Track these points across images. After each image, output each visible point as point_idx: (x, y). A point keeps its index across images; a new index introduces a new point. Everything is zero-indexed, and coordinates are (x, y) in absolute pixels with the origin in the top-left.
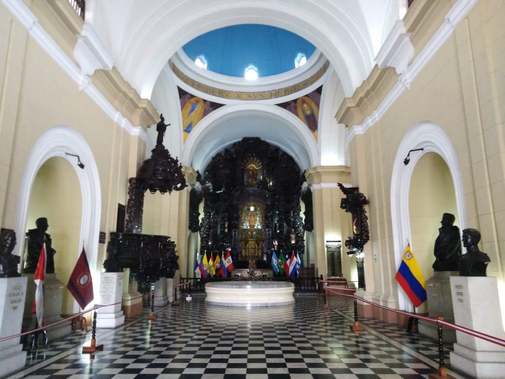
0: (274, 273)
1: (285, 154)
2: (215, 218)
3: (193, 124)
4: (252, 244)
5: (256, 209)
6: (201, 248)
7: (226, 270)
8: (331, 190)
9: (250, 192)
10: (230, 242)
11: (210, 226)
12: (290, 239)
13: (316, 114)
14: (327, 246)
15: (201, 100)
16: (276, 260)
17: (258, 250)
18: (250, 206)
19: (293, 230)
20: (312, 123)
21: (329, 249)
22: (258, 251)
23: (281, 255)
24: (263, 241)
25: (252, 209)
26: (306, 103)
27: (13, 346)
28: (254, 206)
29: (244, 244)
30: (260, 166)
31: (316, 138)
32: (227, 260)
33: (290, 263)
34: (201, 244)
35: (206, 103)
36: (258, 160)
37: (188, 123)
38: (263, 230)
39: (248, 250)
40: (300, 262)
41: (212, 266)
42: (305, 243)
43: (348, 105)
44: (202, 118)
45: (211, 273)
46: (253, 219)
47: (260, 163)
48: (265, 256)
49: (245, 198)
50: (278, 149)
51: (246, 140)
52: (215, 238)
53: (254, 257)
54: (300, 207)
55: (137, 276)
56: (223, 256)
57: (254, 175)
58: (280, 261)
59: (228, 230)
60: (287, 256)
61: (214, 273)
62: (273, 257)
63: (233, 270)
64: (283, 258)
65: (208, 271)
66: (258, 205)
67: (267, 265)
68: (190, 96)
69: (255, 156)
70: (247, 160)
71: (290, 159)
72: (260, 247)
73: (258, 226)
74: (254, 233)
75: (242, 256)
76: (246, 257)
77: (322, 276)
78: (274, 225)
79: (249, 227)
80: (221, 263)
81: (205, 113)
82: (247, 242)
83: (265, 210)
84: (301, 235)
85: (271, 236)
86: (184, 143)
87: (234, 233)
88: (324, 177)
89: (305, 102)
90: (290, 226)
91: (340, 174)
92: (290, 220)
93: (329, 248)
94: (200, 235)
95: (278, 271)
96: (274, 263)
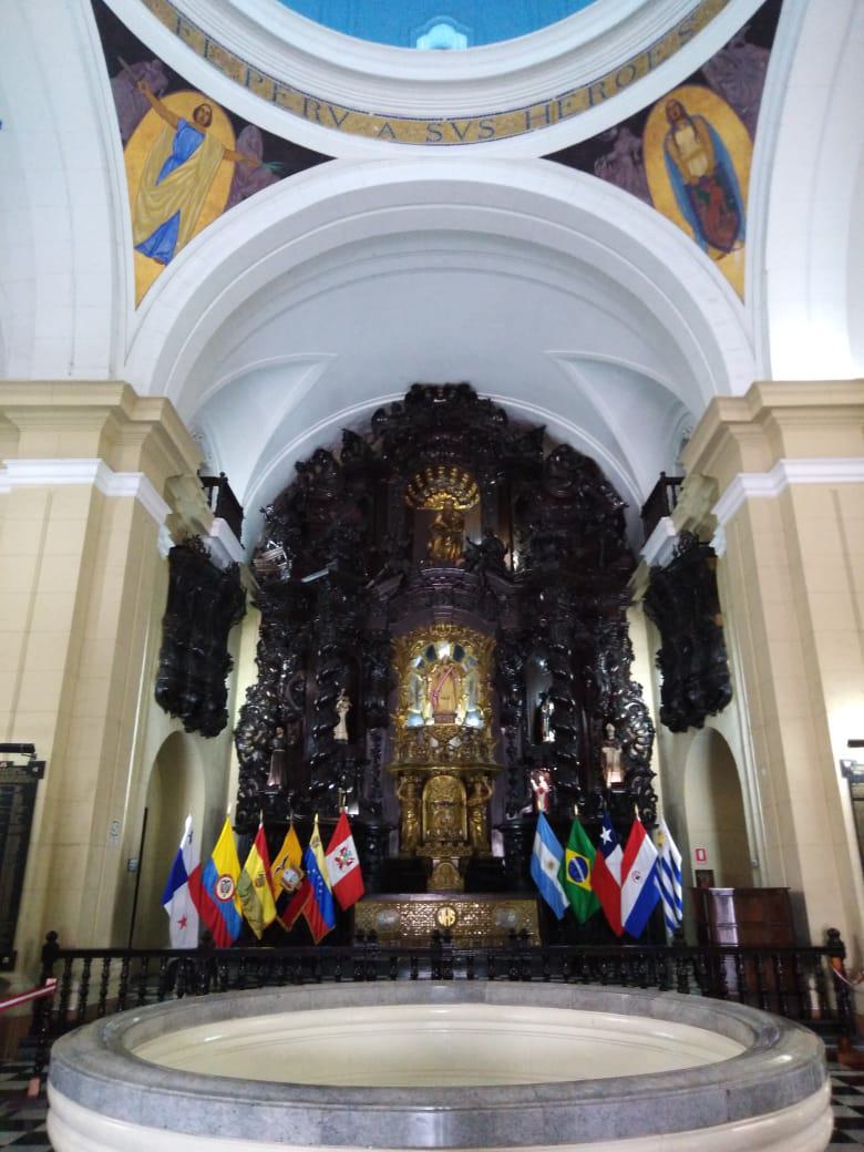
0: (546, 912)
1: (566, 451)
2: (296, 684)
3: (185, 229)
4: (443, 786)
5: (458, 654)
6: (239, 808)
7: (329, 902)
8: (835, 493)
9: (438, 586)
10: (357, 783)
11: (277, 715)
12: (598, 766)
14: (846, 772)
16: (554, 853)
18: (436, 639)
19: (611, 727)
20: (716, 213)
22: (470, 816)
23: (578, 829)
24: (488, 774)
25: (445, 651)
26: (690, 121)
27: (106, 976)
28: (451, 639)
29: (410, 789)
30: (473, 497)
32: (336, 853)
33: (626, 866)
34: (242, 789)
36: (466, 478)
37: (165, 214)
38: (489, 734)
39: (430, 815)
41: (260, 883)
42: (656, 783)
43: (725, 416)
45: (253, 915)
46: (447, 687)
47: (474, 487)
48: (500, 836)
50: (536, 434)
51: (418, 394)
53: (455, 845)
54: (630, 644)
55: (467, 862)
56: (316, 833)
58: (571, 855)
59: (349, 729)
60: (606, 835)
61: (270, 915)
62: (538, 837)
63: (361, 899)
64: (588, 843)
65: (238, 908)
66: (468, 636)
68: (163, 81)
69: (454, 461)
71: (589, 467)
72: (478, 799)
73: (469, 716)
74: (453, 742)
76: (421, 843)
79: (431, 723)
80: (304, 865)
81: (241, 189)
82: (427, 777)
83: (495, 653)
85: (519, 755)
86: (137, 306)
87: (370, 744)
88: (790, 438)
89: (684, 115)
90: (597, 716)
92: (599, 689)
95: (566, 903)
96: (543, 866)
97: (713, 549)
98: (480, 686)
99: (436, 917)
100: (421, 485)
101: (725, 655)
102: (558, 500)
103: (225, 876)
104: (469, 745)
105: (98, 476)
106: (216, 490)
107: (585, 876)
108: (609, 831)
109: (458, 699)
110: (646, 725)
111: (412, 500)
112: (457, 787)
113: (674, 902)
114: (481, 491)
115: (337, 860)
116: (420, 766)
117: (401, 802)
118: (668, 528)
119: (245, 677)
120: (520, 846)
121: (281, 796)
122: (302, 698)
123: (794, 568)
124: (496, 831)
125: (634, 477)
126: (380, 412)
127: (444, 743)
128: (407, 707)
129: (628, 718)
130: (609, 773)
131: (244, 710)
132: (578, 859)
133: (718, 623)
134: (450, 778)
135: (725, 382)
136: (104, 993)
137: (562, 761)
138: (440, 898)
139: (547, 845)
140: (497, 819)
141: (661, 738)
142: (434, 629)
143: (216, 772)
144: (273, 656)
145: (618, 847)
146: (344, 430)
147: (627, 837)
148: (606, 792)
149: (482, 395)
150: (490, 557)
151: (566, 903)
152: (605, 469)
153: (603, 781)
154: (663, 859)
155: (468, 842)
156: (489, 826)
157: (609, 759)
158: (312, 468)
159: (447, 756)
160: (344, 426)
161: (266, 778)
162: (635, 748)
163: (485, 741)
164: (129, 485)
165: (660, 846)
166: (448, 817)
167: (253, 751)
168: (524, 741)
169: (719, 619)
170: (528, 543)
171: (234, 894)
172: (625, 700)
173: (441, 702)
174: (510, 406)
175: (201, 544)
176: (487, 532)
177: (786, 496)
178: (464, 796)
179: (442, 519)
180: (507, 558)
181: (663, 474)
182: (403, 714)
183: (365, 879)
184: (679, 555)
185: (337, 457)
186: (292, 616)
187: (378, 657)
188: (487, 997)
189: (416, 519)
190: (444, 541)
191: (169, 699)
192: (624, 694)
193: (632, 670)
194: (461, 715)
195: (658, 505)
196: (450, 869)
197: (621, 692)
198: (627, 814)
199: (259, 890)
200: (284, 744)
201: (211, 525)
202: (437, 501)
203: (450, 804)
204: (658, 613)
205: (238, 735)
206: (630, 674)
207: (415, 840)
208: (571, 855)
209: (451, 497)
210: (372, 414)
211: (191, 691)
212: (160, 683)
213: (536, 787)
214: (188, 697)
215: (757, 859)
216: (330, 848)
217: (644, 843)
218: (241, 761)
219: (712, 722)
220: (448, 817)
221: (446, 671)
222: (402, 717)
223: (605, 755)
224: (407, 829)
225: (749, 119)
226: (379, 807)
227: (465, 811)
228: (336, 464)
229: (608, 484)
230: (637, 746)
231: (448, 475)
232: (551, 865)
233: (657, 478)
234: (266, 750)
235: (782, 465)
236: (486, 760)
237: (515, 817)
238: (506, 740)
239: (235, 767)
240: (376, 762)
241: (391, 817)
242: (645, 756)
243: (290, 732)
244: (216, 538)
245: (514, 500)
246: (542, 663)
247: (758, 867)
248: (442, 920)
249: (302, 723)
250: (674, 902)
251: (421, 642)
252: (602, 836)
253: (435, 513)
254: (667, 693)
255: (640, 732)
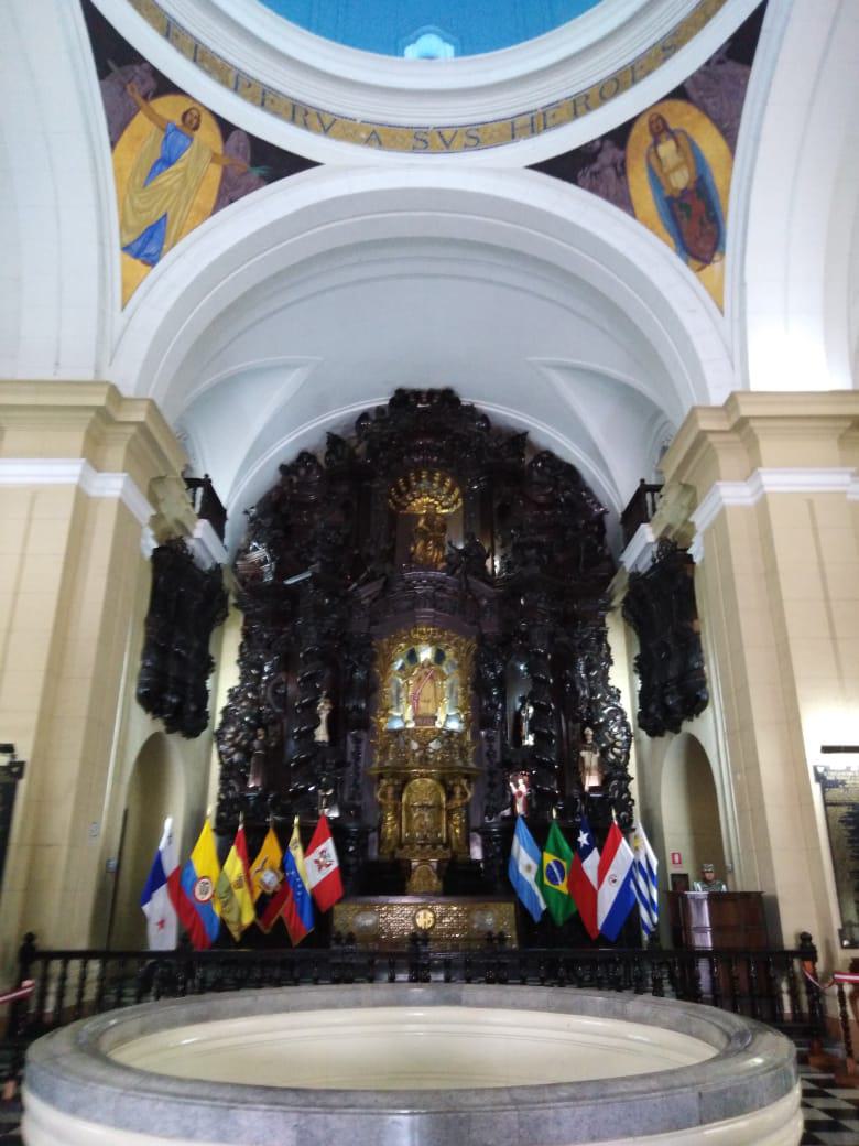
0: (523, 914)
1: (548, 458)
2: (277, 686)
3: (172, 230)
4: (423, 789)
5: (439, 657)
6: (220, 809)
8: (810, 503)
9: (420, 590)
10: (337, 785)
11: (258, 716)
12: (576, 770)
13: (718, 180)
14: (820, 778)
15: (206, 120)
16: (531, 854)
17: (450, 813)
18: (418, 642)
19: (589, 732)
20: (697, 225)
21: (834, 794)
22: (449, 818)
23: (556, 832)
24: (467, 777)
25: (426, 654)
26: (672, 135)
27: (83, 977)
28: (432, 642)
29: (390, 791)
30: (456, 502)
31: (717, 297)
32: (315, 855)
35: (234, 135)
36: (448, 482)
38: (469, 738)
39: (409, 817)
40: (655, 863)
41: (239, 885)
42: (633, 787)
43: (704, 425)
44: (216, 209)
45: (231, 917)
46: (427, 690)
47: (457, 492)
48: (478, 838)
49: (394, 612)
50: (519, 440)
51: (402, 398)
52: (273, 765)
53: (434, 847)
54: (609, 648)
55: (446, 865)
56: (296, 835)
57: (437, 527)
58: (549, 859)
59: (331, 730)
60: (583, 839)
61: (248, 917)
62: (516, 841)
63: (340, 901)
64: (566, 847)
65: (217, 909)
66: (449, 640)
67: (490, 880)
68: (151, 84)
69: (438, 466)
70: (407, 483)
71: (570, 473)
73: (449, 718)
74: (434, 745)
75: (381, 842)
76: (401, 845)
77: (805, 938)
78: (510, 716)
79: (411, 725)
81: (229, 193)
82: (407, 780)
84: (618, 757)
85: (498, 760)
87: (351, 746)
88: (767, 447)
89: (665, 128)
90: (576, 720)
91: (842, 438)
92: (578, 693)
93: (835, 784)
94: (220, 753)
95: (543, 906)
96: (521, 869)
97: (691, 556)
98: (460, 689)
99: (414, 919)
100: (404, 489)
101: (701, 660)
102: (540, 506)
103: (204, 877)
104: (449, 748)
105: (82, 476)
106: (200, 491)
107: (563, 880)
108: (586, 835)
109: (438, 701)
110: (624, 729)
111: (395, 503)
112: (436, 790)
113: (649, 905)
114: (463, 495)
115: (317, 861)
116: (399, 769)
117: (381, 806)
118: (647, 535)
119: (226, 679)
120: (498, 849)
121: (261, 798)
122: (282, 700)
123: (770, 573)
124: (475, 834)
125: (615, 485)
126: (364, 416)
127: (424, 746)
128: (387, 709)
129: (606, 722)
130: (587, 777)
131: (225, 711)
132: (556, 862)
133: (696, 629)
134: (429, 781)
135: (704, 391)
136: (81, 994)
137: (541, 765)
138: (418, 900)
139: (525, 847)
140: (476, 822)
141: (638, 743)
142: (416, 632)
143: (197, 773)
144: (255, 657)
145: (595, 851)
146: (328, 433)
147: (604, 841)
148: (584, 796)
149: (465, 401)
150: (471, 561)
151: (543, 906)
152: (586, 476)
153: (581, 785)
154: (639, 863)
155: (447, 845)
156: (468, 830)
157: (587, 763)
158: (297, 470)
159: (427, 759)
160: (328, 428)
161: (246, 780)
162: (614, 753)
163: (465, 744)
164: (113, 485)
165: (636, 850)
166: (427, 820)
167: (234, 753)
168: (504, 746)
169: (697, 625)
170: (509, 548)
171: (213, 896)
172: (604, 705)
173: (422, 704)
174: (496, 413)
175: (184, 546)
176: (468, 536)
177: (763, 505)
178: (444, 799)
179: (426, 523)
180: (488, 563)
181: (642, 481)
182: (384, 716)
183: (344, 881)
184: (657, 561)
185: (321, 460)
186: (275, 621)
187: (360, 662)
188: (463, 1001)
189: (399, 524)
190: (425, 546)
191: (151, 700)
192: (603, 699)
193: (610, 674)
194: (441, 718)
195: (637, 512)
196: (429, 872)
197: (599, 696)
198: (603, 818)
199: (238, 893)
200: (264, 745)
201: (195, 527)
202: (420, 504)
203: (429, 807)
204: (639, 619)
205: (219, 736)
206: (609, 678)
207: (394, 843)
208: (549, 859)
209: (434, 500)
210: (356, 419)
211: (172, 691)
212: (141, 684)
213: (514, 790)
214: (169, 698)
215: (732, 863)
216: (310, 848)
217: (621, 846)
218: (222, 763)
219: (688, 727)
220: (427, 820)
221: (427, 674)
222: (382, 720)
223: (583, 759)
224: (385, 833)
225: (730, 134)
226: (358, 809)
227: (444, 814)
228: (320, 467)
229: (588, 490)
230: (615, 750)
231: (431, 480)
232: (529, 868)
233: (638, 485)
234: (247, 752)
235: (759, 474)
236: (465, 762)
237: (493, 820)
238: (485, 744)
239: (216, 768)
240: (356, 764)
241: (370, 820)
242: (622, 760)
243: (271, 733)
244: (199, 540)
245: (496, 504)
246: (522, 667)
247: (732, 871)
248: (421, 922)
249: (282, 724)
250: (649, 905)
251: (402, 645)
252: (580, 839)
253: (417, 517)
254: (645, 697)
255: (618, 737)
